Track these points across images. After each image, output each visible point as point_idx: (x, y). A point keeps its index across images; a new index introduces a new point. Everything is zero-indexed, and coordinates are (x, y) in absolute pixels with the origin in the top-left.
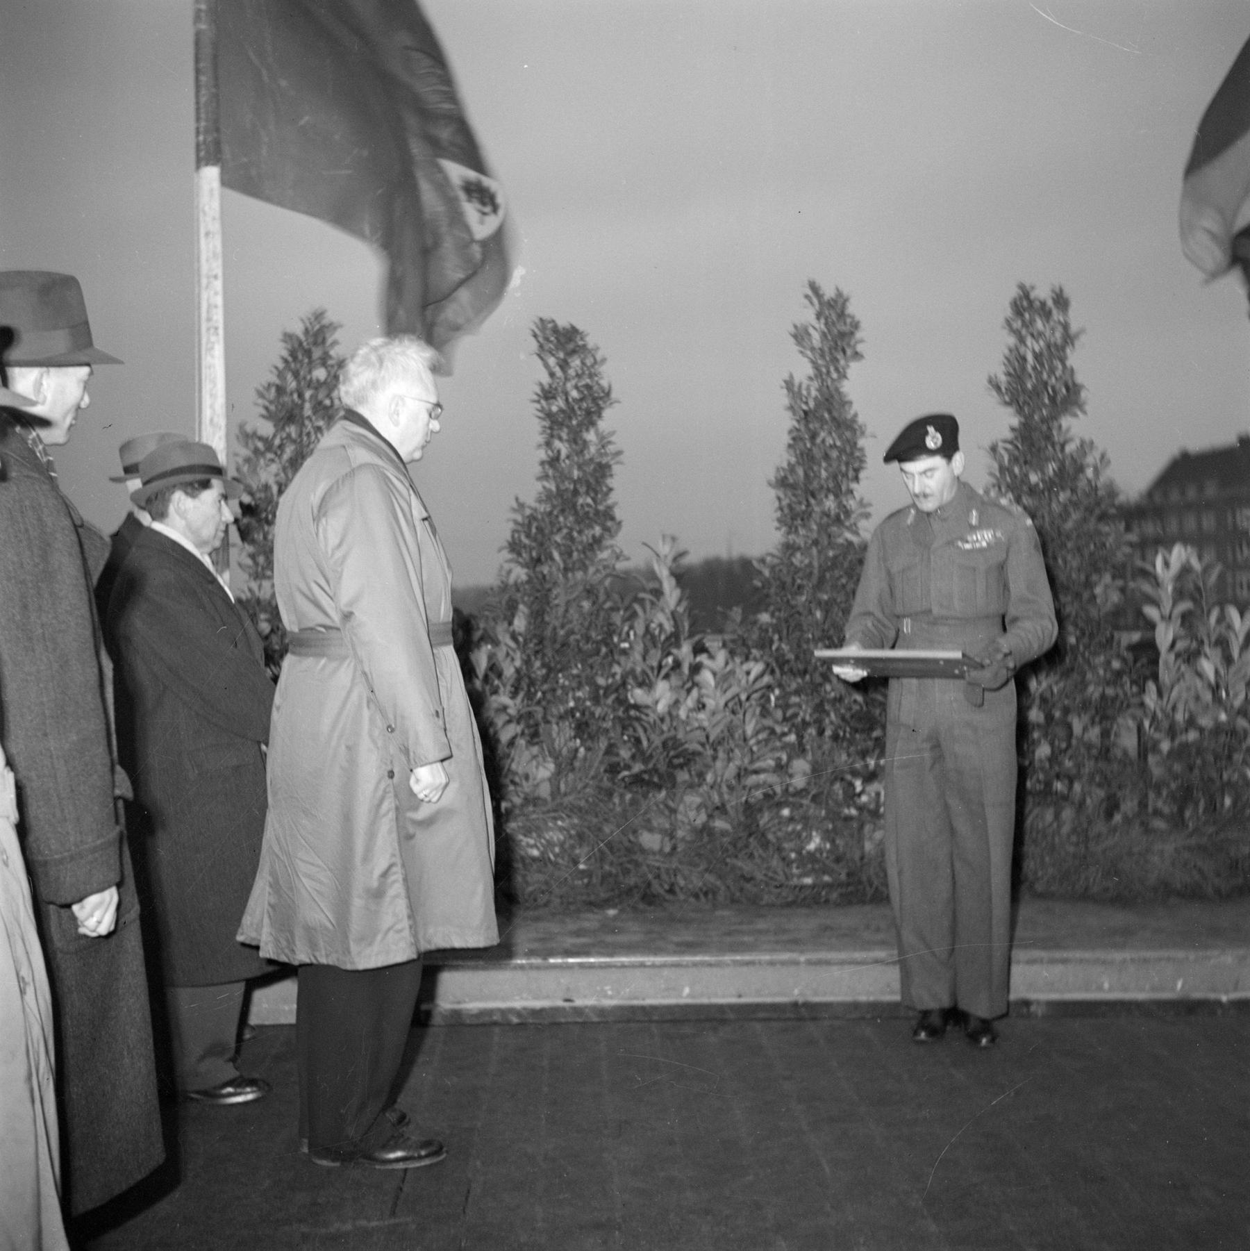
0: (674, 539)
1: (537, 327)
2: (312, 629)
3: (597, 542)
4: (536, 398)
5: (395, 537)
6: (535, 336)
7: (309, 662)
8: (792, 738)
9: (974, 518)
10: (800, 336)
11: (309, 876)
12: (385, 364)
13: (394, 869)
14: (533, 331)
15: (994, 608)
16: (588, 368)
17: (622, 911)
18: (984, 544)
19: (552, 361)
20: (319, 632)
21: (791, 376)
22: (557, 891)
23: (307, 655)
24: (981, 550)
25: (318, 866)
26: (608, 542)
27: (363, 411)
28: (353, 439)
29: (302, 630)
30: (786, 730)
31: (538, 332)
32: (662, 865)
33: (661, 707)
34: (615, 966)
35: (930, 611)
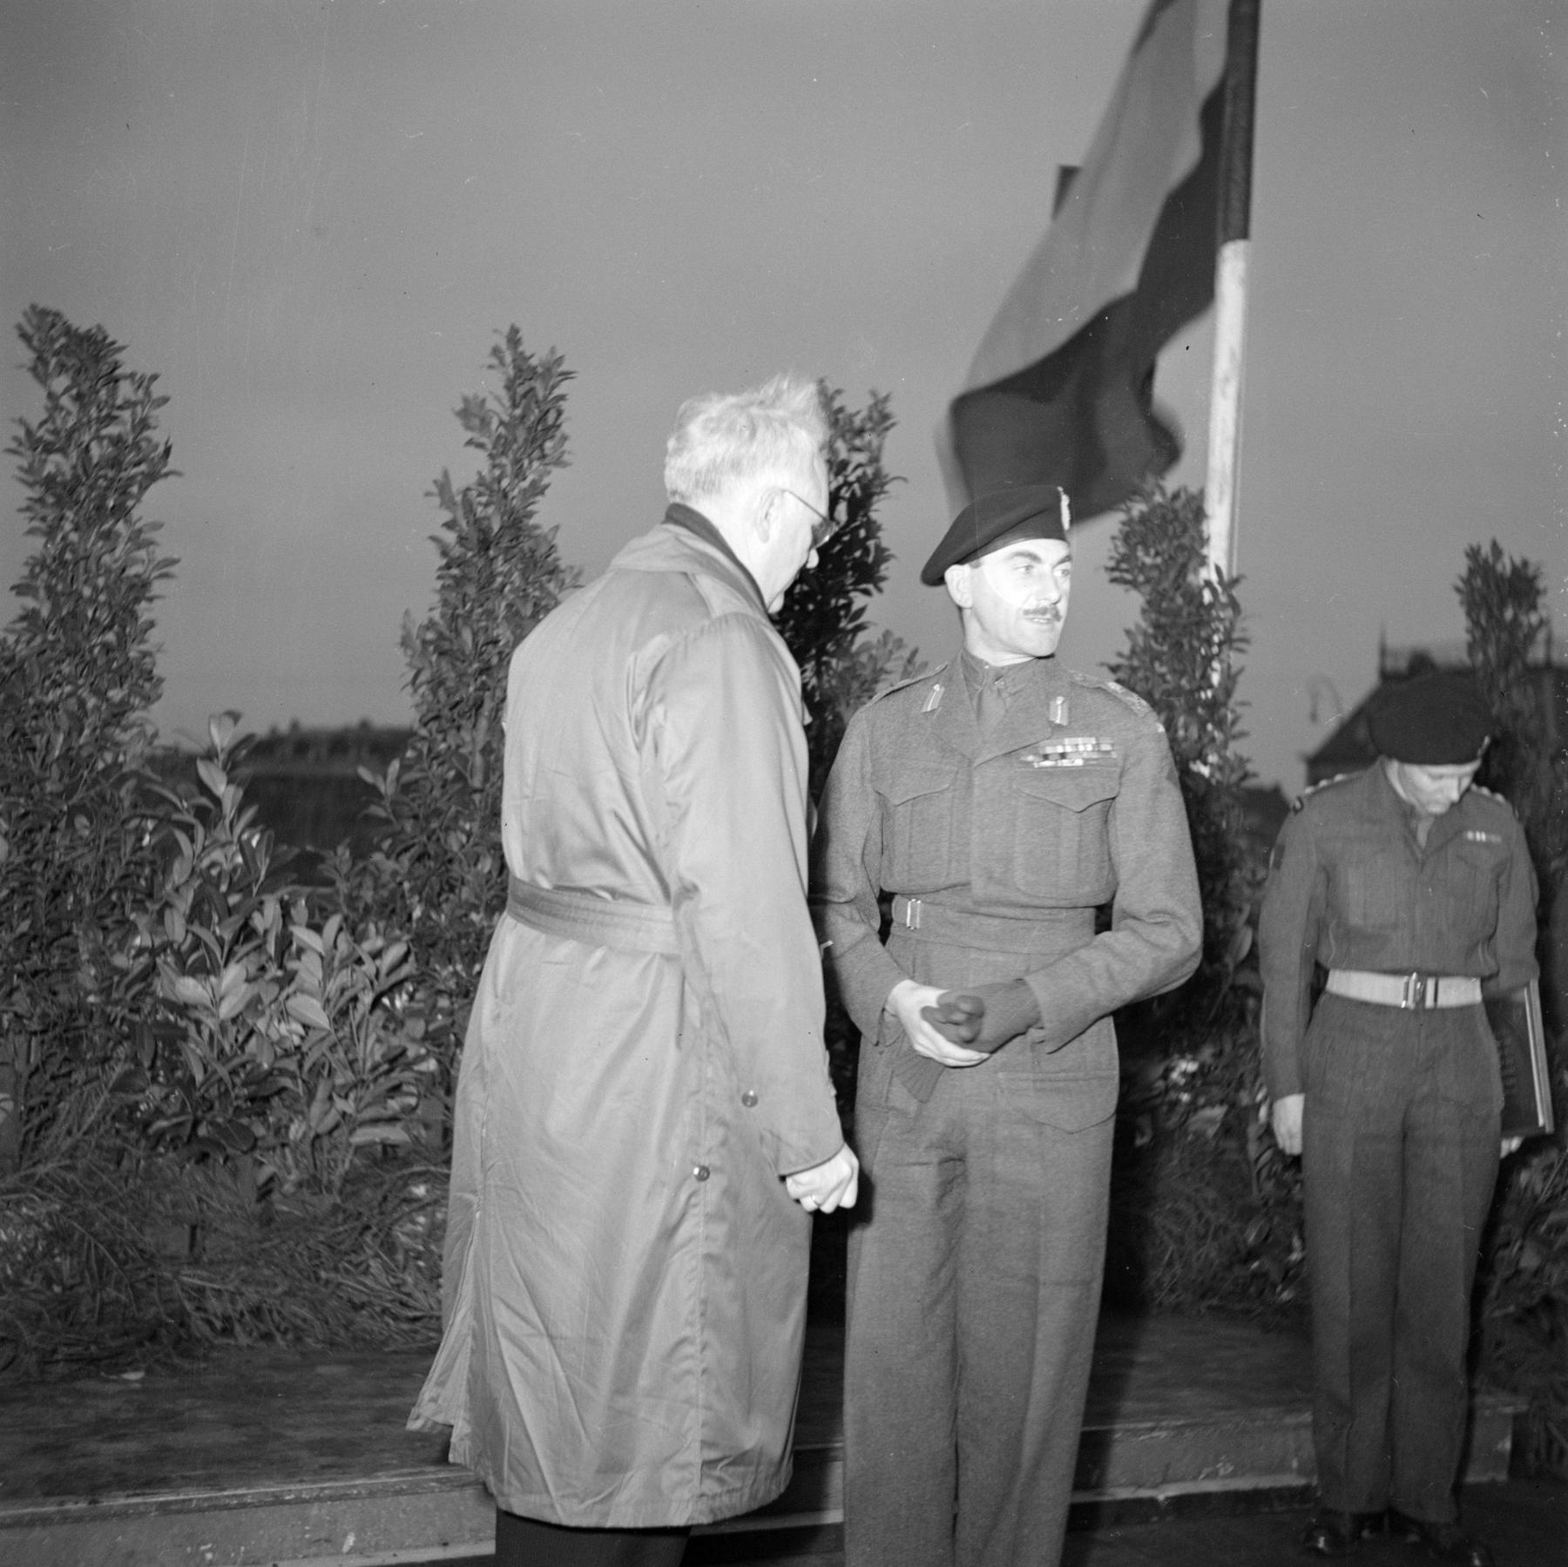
0: (235, 717)
1: (29, 321)
2: (585, 891)
3: (118, 714)
4: (13, 445)
5: (777, 736)
6: (25, 337)
7: (566, 949)
8: (431, 1065)
9: (1059, 714)
10: (471, 413)
11: (513, 1339)
12: (759, 435)
13: (688, 1349)
14: (19, 327)
15: (1092, 893)
16: (113, 406)
17: (149, 1371)
18: (1079, 762)
19: (61, 383)
20: (599, 897)
21: (446, 474)
22: (29, 1338)
23: (567, 936)
24: (1071, 772)
25: (534, 1327)
26: (133, 716)
27: (705, 507)
28: (701, 564)
29: (558, 888)
30: (423, 1051)
31: (29, 330)
32: (208, 1285)
33: (226, 1010)
34: (227, 1507)
35: (966, 885)
